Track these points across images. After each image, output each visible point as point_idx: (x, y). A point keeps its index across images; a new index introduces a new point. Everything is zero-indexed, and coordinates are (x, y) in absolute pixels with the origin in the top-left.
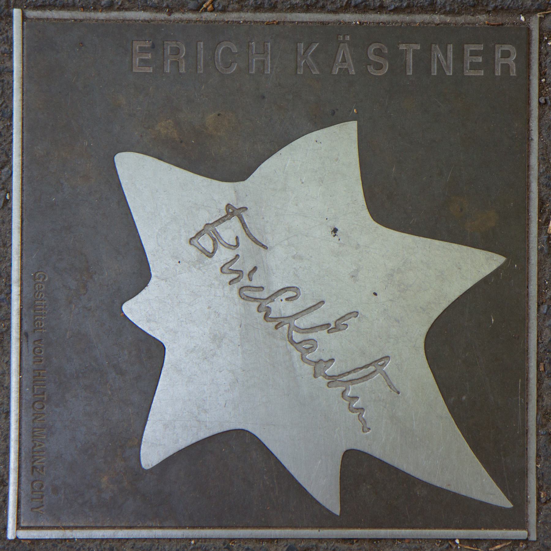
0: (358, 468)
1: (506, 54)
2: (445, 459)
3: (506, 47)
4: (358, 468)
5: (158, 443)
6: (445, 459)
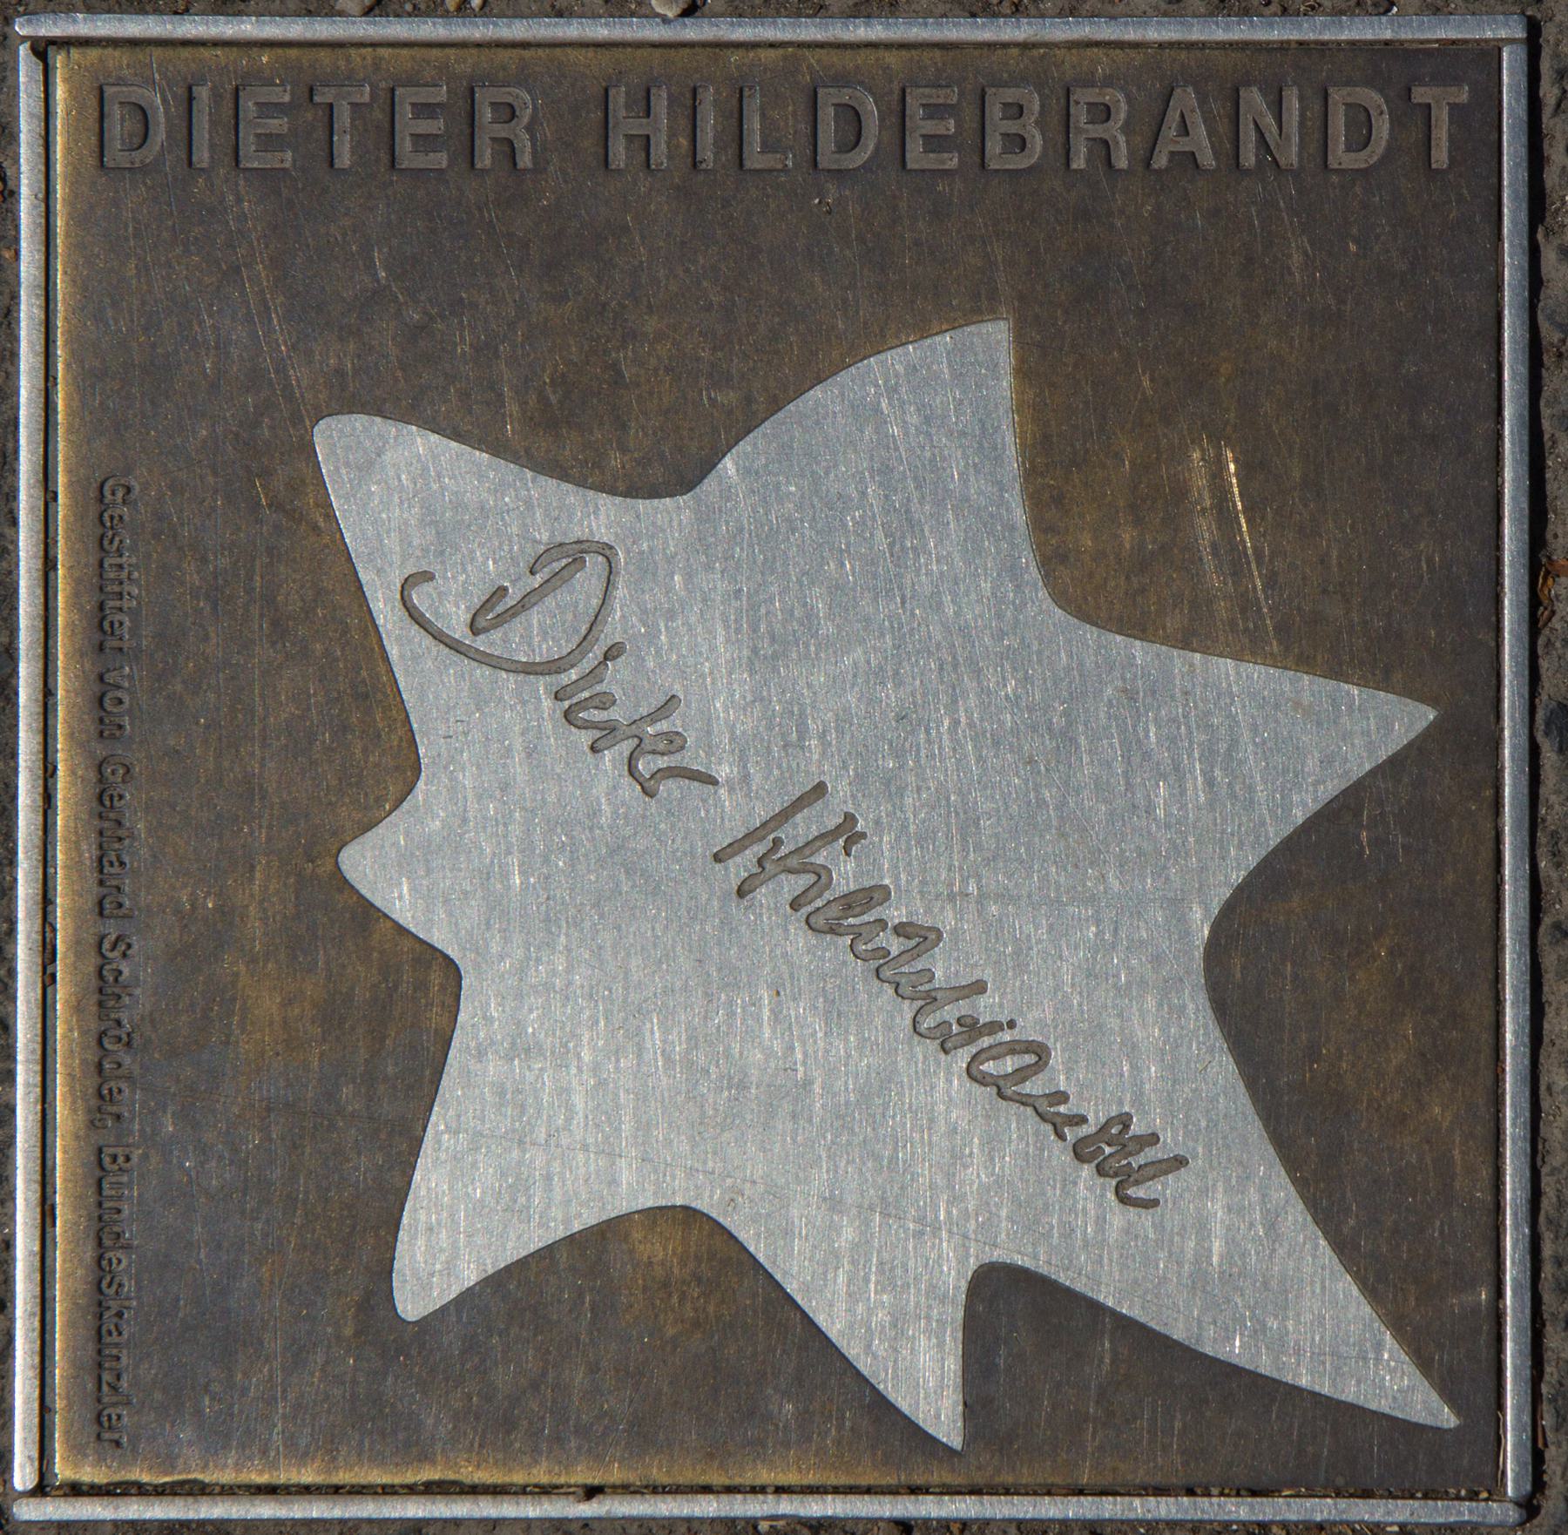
0: (1014, 1314)
1: (1104, 113)
2: (1252, 1271)
3: (1011, 95)
4: (1014, 1314)
5: (450, 1238)
6: (1252, 1271)
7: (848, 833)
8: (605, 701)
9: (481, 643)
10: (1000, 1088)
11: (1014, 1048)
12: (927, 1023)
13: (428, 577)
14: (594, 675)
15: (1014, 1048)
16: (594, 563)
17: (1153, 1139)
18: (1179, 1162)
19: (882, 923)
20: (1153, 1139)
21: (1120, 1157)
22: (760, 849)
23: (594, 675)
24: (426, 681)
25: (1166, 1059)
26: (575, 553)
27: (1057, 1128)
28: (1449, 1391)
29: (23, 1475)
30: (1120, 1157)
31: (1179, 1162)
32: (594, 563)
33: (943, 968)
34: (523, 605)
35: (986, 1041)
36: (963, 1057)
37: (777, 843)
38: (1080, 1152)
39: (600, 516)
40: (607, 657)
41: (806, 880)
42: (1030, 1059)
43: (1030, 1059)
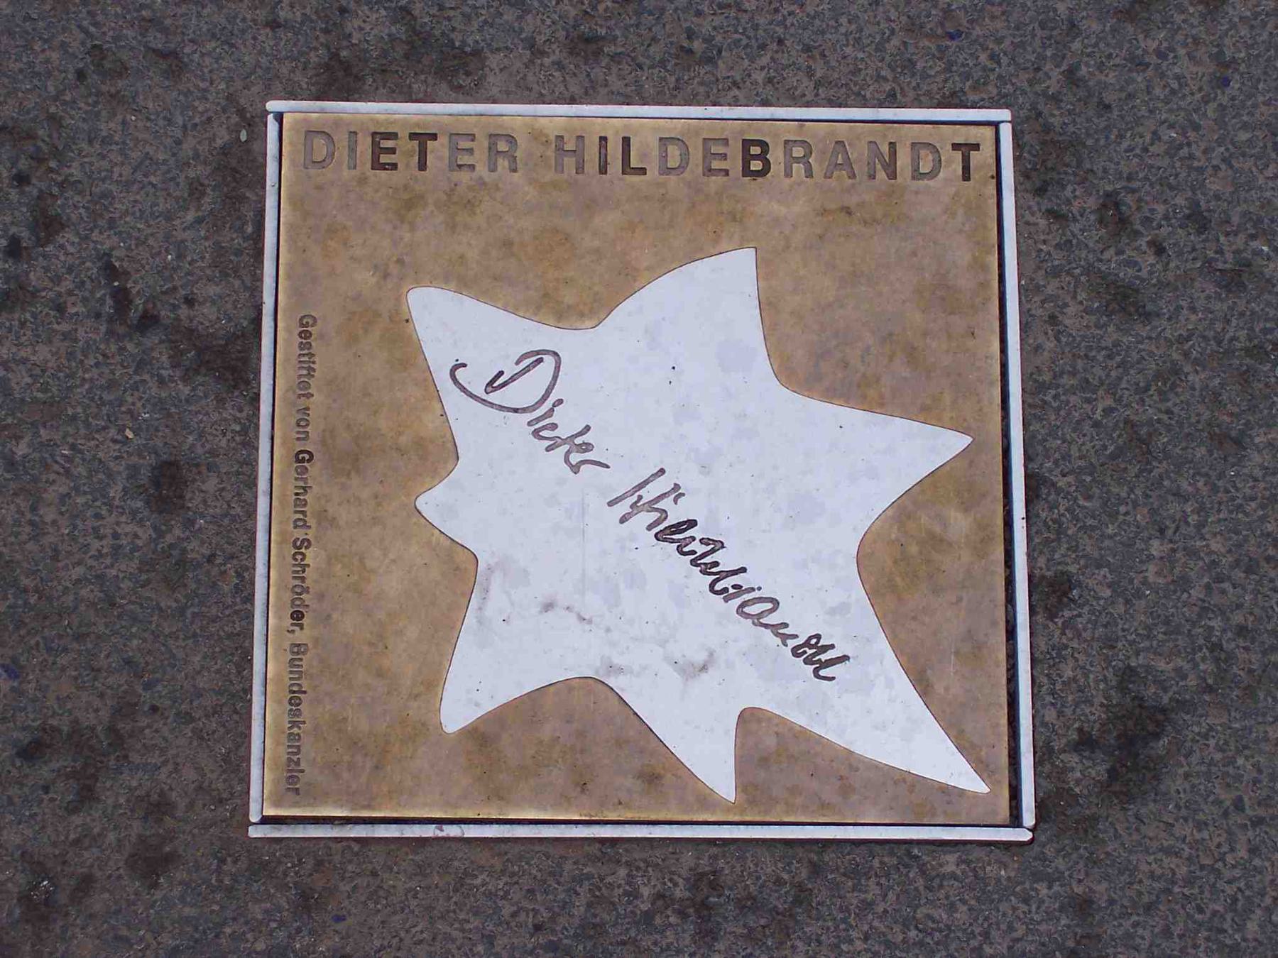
7: (676, 492)
8: (554, 426)
9: (494, 397)
10: (757, 620)
11: (761, 600)
12: (718, 587)
13: (464, 365)
14: (550, 413)
15: (761, 600)
16: (549, 361)
17: (832, 646)
18: (845, 658)
19: (693, 539)
20: (832, 646)
21: (816, 654)
22: (634, 498)
23: (550, 413)
24: (463, 417)
25: (828, 597)
26: (536, 357)
27: (785, 638)
28: (982, 767)
29: (1006, 132)
30: (816, 654)
31: (845, 658)
32: (549, 361)
33: (726, 560)
34: (512, 379)
35: (746, 597)
36: (736, 602)
37: (640, 498)
38: (796, 652)
39: (543, 336)
40: (554, 406)
41: (655, 515)
42: (770, 606)
43: (770, 606)
